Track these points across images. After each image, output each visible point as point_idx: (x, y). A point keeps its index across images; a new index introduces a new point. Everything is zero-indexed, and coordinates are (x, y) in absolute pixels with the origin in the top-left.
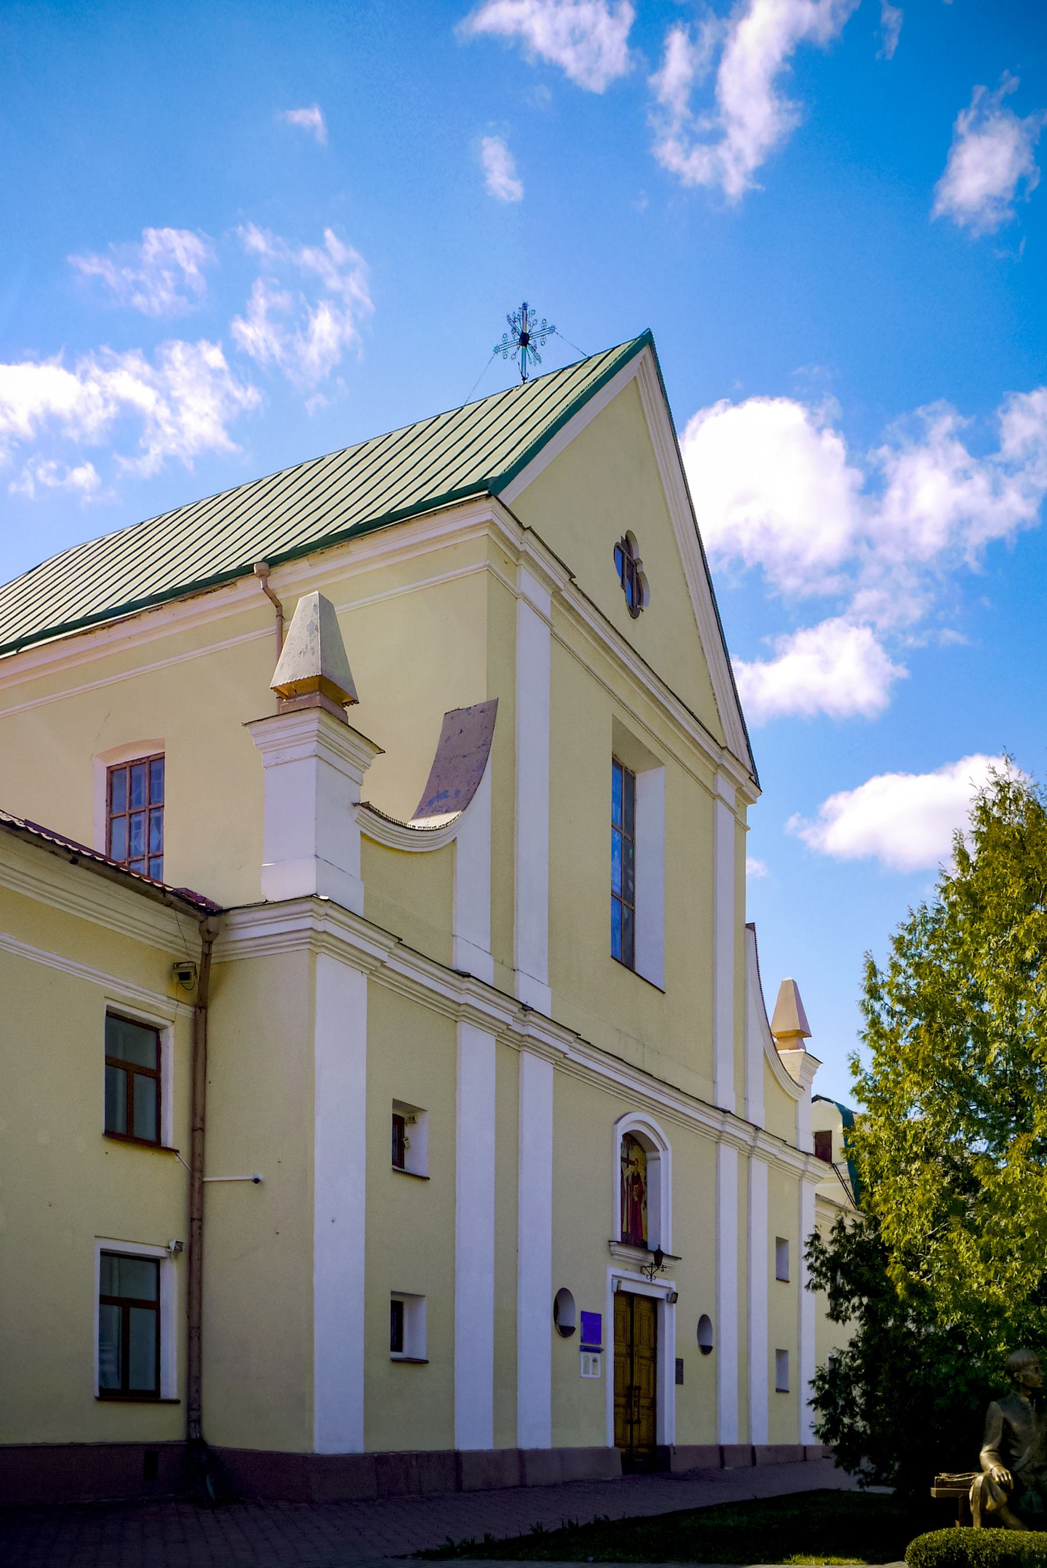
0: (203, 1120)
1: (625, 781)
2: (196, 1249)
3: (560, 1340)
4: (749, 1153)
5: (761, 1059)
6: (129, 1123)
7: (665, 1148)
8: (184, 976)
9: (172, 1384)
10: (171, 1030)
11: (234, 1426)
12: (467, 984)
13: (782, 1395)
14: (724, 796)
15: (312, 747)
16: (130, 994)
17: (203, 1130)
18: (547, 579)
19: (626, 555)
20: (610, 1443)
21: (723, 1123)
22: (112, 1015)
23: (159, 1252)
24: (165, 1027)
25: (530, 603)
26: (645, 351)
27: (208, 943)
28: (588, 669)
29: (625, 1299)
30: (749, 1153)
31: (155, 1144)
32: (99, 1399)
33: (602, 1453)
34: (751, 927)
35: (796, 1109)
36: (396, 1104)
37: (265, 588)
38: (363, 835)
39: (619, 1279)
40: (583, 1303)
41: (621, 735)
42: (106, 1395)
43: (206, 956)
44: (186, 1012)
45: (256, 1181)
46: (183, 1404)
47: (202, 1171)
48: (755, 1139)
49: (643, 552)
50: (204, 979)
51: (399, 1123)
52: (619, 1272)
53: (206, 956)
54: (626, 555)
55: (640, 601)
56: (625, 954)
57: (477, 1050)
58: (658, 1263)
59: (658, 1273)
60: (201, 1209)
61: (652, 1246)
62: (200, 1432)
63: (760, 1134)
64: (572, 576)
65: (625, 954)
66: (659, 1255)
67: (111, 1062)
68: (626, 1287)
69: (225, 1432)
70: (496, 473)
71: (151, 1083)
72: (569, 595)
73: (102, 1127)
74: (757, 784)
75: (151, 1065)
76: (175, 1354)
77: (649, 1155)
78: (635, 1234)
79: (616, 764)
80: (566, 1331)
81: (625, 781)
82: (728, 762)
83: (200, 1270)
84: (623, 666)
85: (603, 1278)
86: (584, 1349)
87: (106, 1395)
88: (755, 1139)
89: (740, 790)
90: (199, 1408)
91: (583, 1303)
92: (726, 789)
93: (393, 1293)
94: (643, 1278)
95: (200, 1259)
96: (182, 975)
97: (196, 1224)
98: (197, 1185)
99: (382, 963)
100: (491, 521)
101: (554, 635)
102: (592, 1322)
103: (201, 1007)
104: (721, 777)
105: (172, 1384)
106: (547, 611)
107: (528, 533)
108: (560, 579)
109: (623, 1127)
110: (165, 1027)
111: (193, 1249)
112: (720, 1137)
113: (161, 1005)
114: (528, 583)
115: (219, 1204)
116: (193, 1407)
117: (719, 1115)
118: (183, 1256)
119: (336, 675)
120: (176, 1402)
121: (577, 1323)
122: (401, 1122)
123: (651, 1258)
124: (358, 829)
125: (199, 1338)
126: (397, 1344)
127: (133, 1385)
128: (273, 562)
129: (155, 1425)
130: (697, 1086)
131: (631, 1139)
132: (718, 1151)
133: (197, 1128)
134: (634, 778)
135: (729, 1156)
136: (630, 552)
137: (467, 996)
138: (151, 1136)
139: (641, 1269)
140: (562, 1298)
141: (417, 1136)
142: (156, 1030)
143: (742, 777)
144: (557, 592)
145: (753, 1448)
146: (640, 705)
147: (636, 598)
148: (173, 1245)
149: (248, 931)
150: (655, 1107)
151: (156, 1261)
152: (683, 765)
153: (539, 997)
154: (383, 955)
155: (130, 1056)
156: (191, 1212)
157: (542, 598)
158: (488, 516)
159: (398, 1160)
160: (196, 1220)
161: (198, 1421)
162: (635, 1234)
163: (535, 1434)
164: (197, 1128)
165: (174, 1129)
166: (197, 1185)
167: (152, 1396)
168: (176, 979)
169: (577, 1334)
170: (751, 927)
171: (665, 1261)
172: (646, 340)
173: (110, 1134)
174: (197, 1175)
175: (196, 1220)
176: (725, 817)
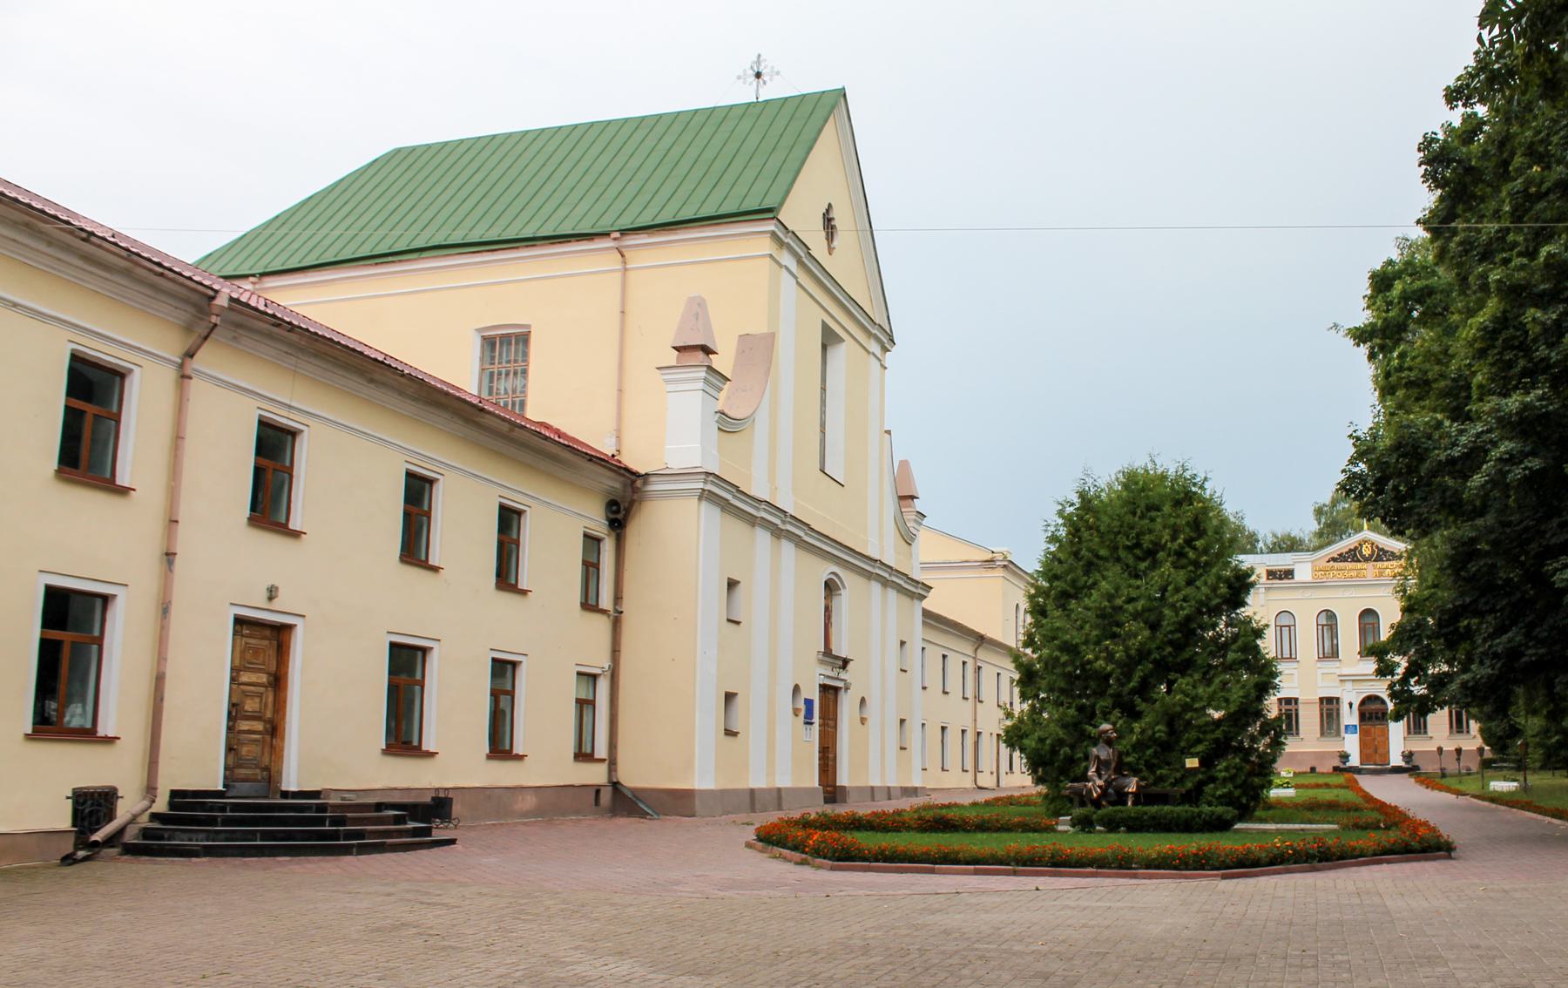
9: (601, 751)
13: (730, 739)
15: (701, 385)
22: (586, 536)
23: (598, 671)
24: (131, 371)
29: (824, 688)
33: (809, 791)
34: (889, 432)
40: (805, 694)
85: (813, 678)
92: (874, 347)
100: (773, 234)
105: (601, 751)
110: (131, 371)
116: (612, 763)
120: (603, 760)
124: (716, 426)
129: (595, 774)
133: (618, 598)
140: (796, 689)
144: (800, 262)
149: (655, 486)
157: (793, 266)
158: (772, 228)
163: (784, 781)
164: (618, 598)
170: (889, 432)
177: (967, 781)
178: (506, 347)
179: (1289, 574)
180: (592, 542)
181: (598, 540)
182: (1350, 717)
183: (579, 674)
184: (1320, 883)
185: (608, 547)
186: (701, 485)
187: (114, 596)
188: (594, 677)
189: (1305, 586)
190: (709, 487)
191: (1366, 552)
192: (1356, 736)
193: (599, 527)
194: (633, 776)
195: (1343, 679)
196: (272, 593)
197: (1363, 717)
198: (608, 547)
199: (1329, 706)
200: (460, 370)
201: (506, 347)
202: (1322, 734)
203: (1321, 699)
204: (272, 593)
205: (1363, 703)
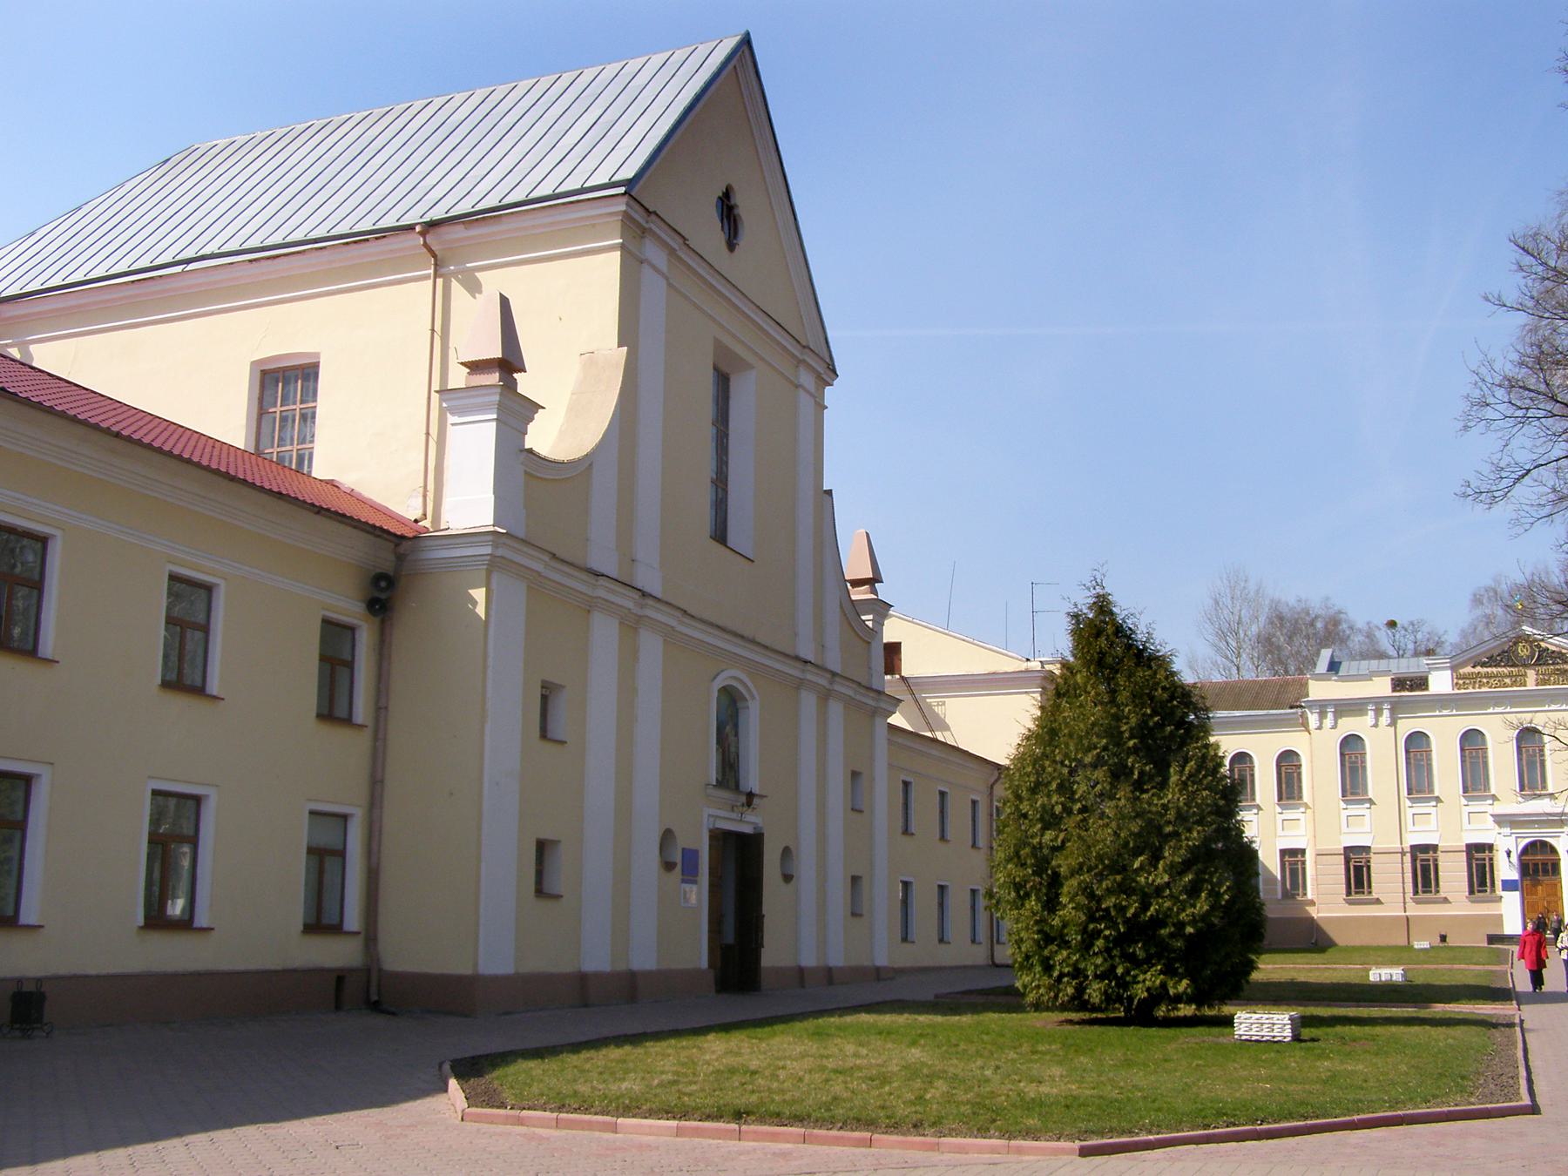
1: (723, 381)
7: (753, 697)
12: (602, 581)
14: (806, 384)
18: (665, 244)
20: (704, 964)
30: (825, 696)
31: (348, 721)
34: (829, 492)
35: (869, 650)
37: (425, 245)
40: (683, 841)
41: (720, 349)
49: (739, 199)
51: (544, 699)
57: (604, 632)
58: (749, 804)
61: (744, 787)
67: (323, 658)
78: (729, 771)
79: (716, 369)
80: (669, 866)
81: (723, 381)
85: (703, 818)
86: (684, 881)
89: (819, 376)
91: (683, 841)
92: (806, 379)
94: (734, 816)
99: (539, 574)
101: (670, 285)
102: (690, 856)
104: (802, 370)
105: (353, 919)
106: (665, 269)
108: (675, 243)
114: (653, 252)
116: (370, 936)
119: (511, 359)
120: (358, 933)
121: (678, 858)
123: (743, 799)
127: (325, 921)
128: (433, 225)
129: (336, 953)
133: (381, 709)
135: (808, 701)
137: (602, 590)
140: (667, 837)
143: (821, 369)
144: (672, 252)
159: (544, 735)
160: (376, 782)
162: (729, 771)
163: (644, 959)
164: (381, 709)
167: (337, 929)
169: (679, 867)
170: (829, 492)
175: (376, 782)
176: (805, 402)
177: (979, 955)
178: (286, 384)
179: (1421, 683)
180: (335, 634)
181: (352, 629)
182: (1506, 870)
183: (312, 813)
184: (537, 1072)
185: (365, 639)
186: (488, 550)
187: (38, 776)
188: (344, 818)
189: (1442, 702)
190: (500, 552)
191: (1523, 651)
192: (1517, 894)
193: (350, 609)
194: (407, 952)
195: (1501, 820)
196: (1443, 938)
197: (1525, 869)
198: (365, 639)
199: (1479, 858)
200: (223, 417)
201: (286, 384)
202: (1471, 892)
203: (1469, 846)
204: (1443, 938)
205: (1525, 851)
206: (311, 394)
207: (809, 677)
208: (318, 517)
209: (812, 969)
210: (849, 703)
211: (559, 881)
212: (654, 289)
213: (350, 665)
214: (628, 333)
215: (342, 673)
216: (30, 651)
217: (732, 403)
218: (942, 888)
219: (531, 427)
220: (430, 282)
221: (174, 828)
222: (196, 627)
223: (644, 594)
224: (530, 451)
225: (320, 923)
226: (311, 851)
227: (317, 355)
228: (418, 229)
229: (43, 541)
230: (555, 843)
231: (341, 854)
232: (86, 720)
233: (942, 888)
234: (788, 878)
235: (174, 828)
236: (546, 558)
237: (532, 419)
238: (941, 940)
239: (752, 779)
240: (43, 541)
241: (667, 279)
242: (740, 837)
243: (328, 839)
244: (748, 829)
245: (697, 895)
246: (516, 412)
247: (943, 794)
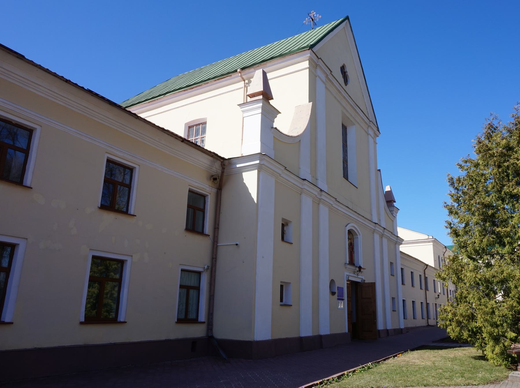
0: (218, 225)
1: (344, 129)
2: (214, 269)
3: (332, 296)
4: (382, 236)
5: (384, 209)
6: (194, 224)
7: (360, 235)
8: (215, 179)
9: (203, 316)
10: (209, 197)
11: (225, 330)
13: (394, 312)
16: (196, 184)
17: (218, 228)
18: (325, 73)
19: (343, 70)
20: (347, 331)
21: (375, 227)
22: (190, 191)
25: (319, 77)
26: (347, 21)
27: (223, 168)
28: (335, 97)
31: (202, 233)
32: (176, 323)
33: (344, 334)
34: (379, 170)
36: (283, 219)
38: (274, 137)
39: (348, 276)
40: (338, 284)
41: (344, 117)
42: (180, 321)
43: (223, 172)
44: (214, 190)
45: (237, 245)
46: (206, 323)
47: (217, 242)
48: (384, 232)
49: (348, 69)
50: (221, 180)
52: (348, 274)
53: (223, 172)
54: (343, 70)
55: (347, 82)
56: (346, 176)
58: (360, 271)
59: (360, 274)
60: (216, 255)
62: (212, 333)
63: (385, 230)
64: (331, 72)
65: (346, 176)
66: (360, 268)
67: (189, 206)
68: (351, 278)
69: (222, 332)
70: (311, 44)
71: (201, 213)
72: (330, 77)
73: (185, 227)
74: (379, 131)
75: (202, 207)
76: (204, 306)
77: (354, 237)
78: (352, 262)
79: (343, 125)
80: (333, 293)
81: (344, 129)
82: (372, 125)
83: (215, 276)
84: (344, 97)
85: (345, 276)
86: (338, 299)
87: (180, 321)
88: (384, 232)
90: (212, 325)
91: (338, 284)
92: (371, 132)
93: (281, 282)
94: (355, 275)
95: (215, 272)
96: (214, 179)
97: (214, 260)
98: (215, 246)
101: (326, 87)
102: (340, 289)
103: (219, 189)
105: (203, 316)
106: (324, 80)
107: (320, 60)
108: (328, 72)
109: (348, 228)
110: (207, 195)
111: (212, 269)
112: (374, 231)
113: (205, 187)
114: (319, 72)
115: (222, 253)
116: (210, 323)
117: (374, 224)
118: (209, 271)
120: (204, 323)
121: (336, 291)
122: (284, 225)
123: (358, 269)
125: (213, 299)
126: (281, 300)
129: (196, 331)
130: (368, 216)
131: (350, 232)
132: (374, 236)
133: (216, 227)
134: (346, 128)
135: (377, 237)
136: (344, 69)
138: (200, 230)
139: (354, 273)
140: (332, 282)
141: (291, 231)
142: (204, 197)
143: (375, 129)
144: (327, 76)
145: (387, 330)
146: (349, 108)
147: (346, 81)
148: (206, 267)
150: (357, 222)
151: (199, 273)
152: (360, 125)
153: (325, 188)
154: (280, 172)
155: (196, 203)
156: (213, 256)
160: (214, 258)
161: (212, 329)
163: (325, 330)
164: (216, 227)
165: (208, 228)
166: (215, 246)
167: (195, 321)
168: (212, 180)
169: (336, 295)
170: (379, 170)
171: (362, 270)
172: (347, 18)
173: (187, 229)
174: (216, 243)
175: (214, 258)
176: (371, 140)
177: (423, 323)
183: (182, 270)
186: (258, 162)
190: (262, 163)
206: (204, 131)
207: (377, 229)
208: (183, 144)
209: (382, 330)
210: (389, 239)
211: (290, 298)
212: (321, 87)
213: (203, 211)
214: (312, 97)
215: (199, 214)
216: (19, 181)
217: (348, 136)
218: (413, 302)
219: (275, 120)
220: (243, 89)
221: (106, 274)
222: (122, 184)
223: (321, 190)
224: (276, 128)
225: (186, 318)
226: (181, 287)
227: (206, 119)
228: (238, 70)
229: (30, 132)
230: (288, 284)
231: (198, 288)
232: (53, 217)
233: (413, 302)
234: (403, 284)
235: (106, 274)
236: (283, 168)
237: (276, 117)
238: (414, 318)
239: (361, 261)
240: (30, 132)
241: (325, 84)
242: (356, 283)
243: (192, 281)
244: (359, 280)
245: (342, 305)
246: (269, 114)
247: (412, 272)
